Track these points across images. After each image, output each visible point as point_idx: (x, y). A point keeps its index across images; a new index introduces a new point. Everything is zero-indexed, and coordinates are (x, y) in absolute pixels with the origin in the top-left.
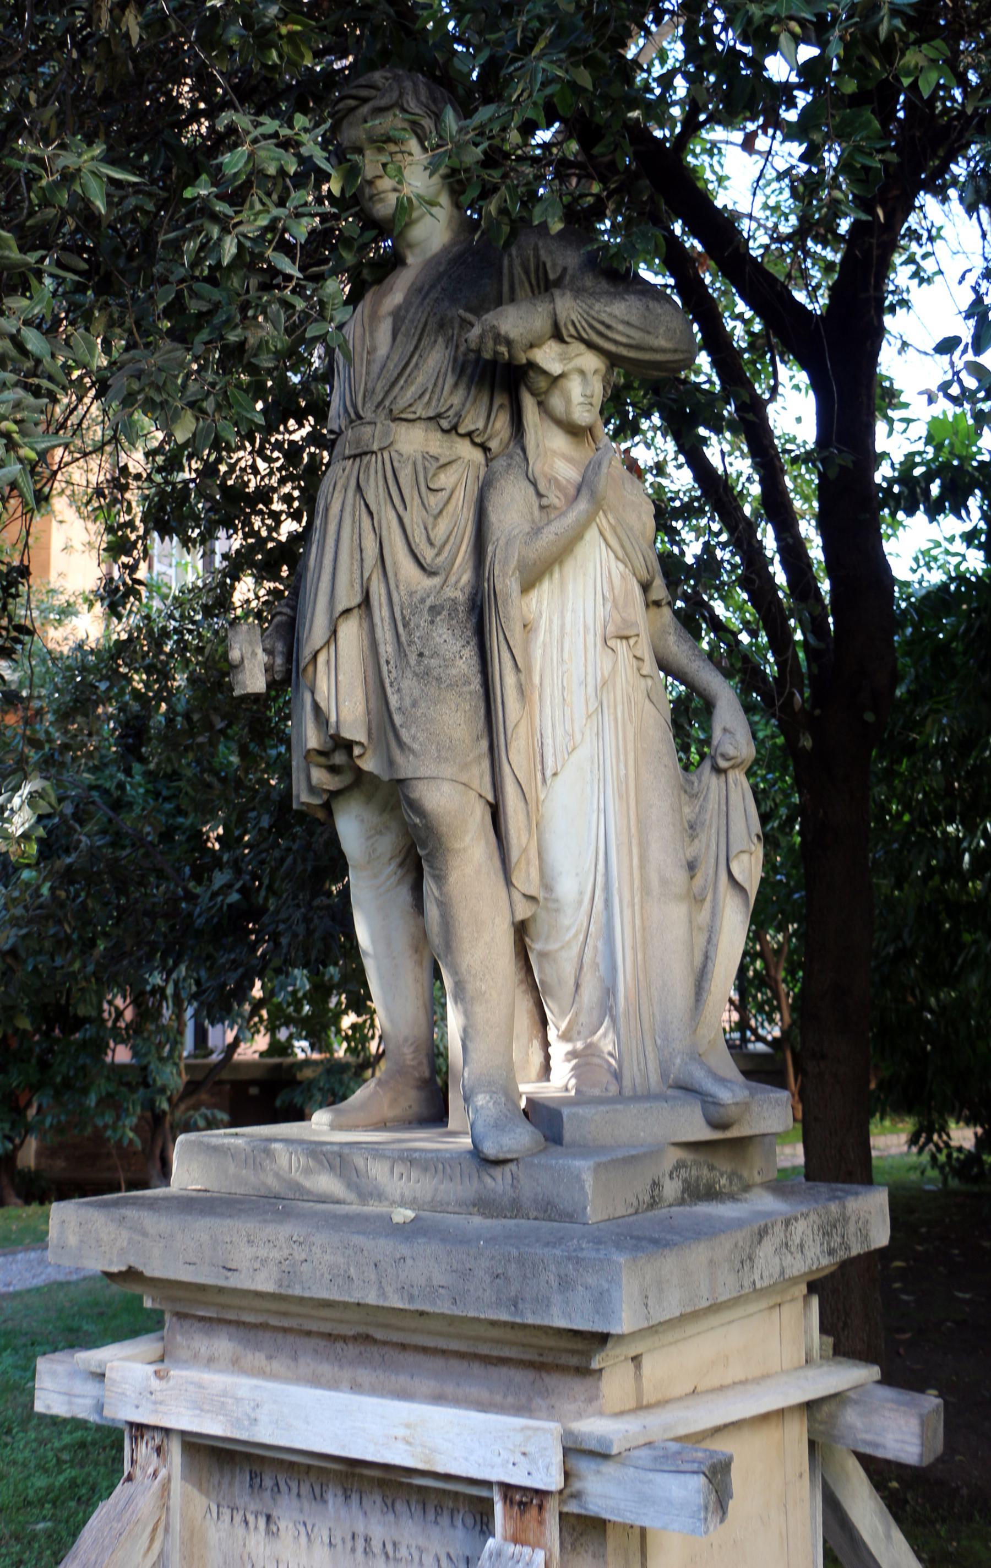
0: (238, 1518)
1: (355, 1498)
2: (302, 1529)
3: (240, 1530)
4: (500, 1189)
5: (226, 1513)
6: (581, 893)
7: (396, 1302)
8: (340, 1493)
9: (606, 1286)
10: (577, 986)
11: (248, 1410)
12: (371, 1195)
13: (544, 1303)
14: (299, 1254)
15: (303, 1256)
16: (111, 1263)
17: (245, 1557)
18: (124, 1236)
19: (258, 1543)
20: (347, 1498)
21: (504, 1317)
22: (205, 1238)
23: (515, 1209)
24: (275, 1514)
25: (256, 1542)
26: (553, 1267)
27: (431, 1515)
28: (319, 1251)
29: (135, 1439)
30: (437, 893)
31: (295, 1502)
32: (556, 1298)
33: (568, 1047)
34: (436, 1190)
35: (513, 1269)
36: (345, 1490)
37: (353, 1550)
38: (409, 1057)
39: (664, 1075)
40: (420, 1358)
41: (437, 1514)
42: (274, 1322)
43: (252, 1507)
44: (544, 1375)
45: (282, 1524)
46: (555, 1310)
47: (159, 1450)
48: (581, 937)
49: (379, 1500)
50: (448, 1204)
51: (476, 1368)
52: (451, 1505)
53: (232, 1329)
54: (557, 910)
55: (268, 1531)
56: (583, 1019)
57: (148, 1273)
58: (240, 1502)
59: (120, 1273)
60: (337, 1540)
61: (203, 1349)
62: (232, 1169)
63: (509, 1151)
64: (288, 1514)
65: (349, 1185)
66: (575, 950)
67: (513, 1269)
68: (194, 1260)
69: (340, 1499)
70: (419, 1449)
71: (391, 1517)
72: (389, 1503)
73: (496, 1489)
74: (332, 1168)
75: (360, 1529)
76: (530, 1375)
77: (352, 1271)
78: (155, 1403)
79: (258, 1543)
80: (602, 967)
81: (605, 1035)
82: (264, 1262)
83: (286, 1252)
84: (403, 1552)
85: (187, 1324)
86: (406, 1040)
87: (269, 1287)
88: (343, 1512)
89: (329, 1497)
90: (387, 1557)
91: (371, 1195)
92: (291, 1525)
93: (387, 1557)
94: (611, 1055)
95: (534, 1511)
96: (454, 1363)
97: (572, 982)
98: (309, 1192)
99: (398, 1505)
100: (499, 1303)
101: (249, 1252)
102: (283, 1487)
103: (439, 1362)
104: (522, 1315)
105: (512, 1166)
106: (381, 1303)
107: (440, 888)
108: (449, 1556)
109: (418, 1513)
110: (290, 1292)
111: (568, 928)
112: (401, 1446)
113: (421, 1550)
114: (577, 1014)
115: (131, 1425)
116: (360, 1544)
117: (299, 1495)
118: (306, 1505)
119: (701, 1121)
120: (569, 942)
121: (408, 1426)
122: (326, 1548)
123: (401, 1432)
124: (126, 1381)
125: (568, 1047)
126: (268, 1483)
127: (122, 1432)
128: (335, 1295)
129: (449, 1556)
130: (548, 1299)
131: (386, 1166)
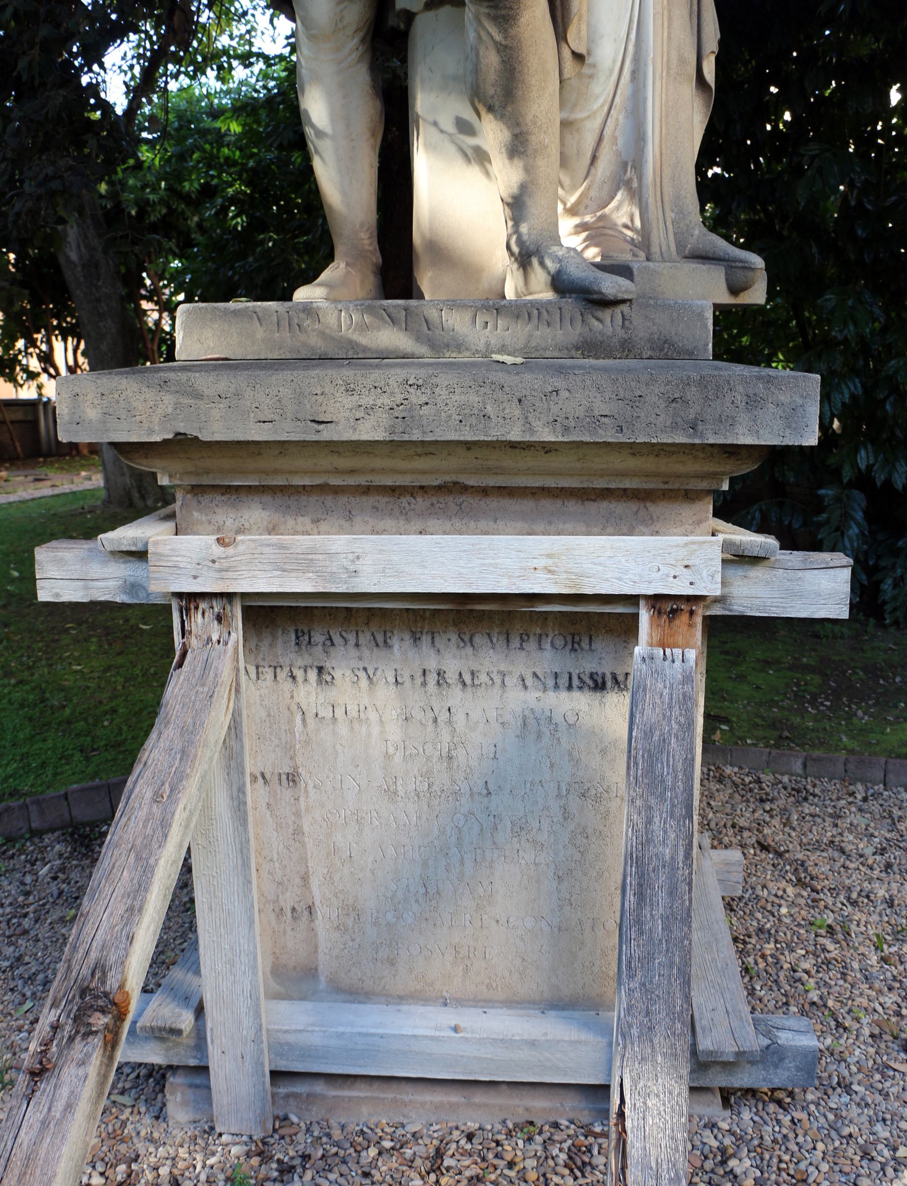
0: (282, 675)
1: (426, 639)
2: (362, 674)
3: (286, 685)
4: (609, 330)
5: (268, 674)
6: (614, 61)
7: (547, 436)
8: (407, 636)
9: (800, 401)
10: (594, 158)
11: (346, 563)
12: (448, 346)
13: (732, 422)
14: (417, 397)
15: (424, 399)
16: (151, 431)
17: (294, 707)
18: (168, 401)
19: (309, 693)
20: (416, 640)
21: (681, 439)
22: (286, 392)
23: (627, 348)
24: (328, 665)
25: (308, 693)
26: (740, 388)
27: (516, 642)
28: (444, 392)
29: (185, 611)
30: (498, 37)
31: (353, 652)
32: (743, 418)
33: (576, 220)
34: (530, 336)
35: (692, 393)
36: (413, 633)
37: (424, 684)
38: (367, 242)
39: (680, 245)
40: (506, 502)
41: (522, 640)
42: (335, 481)
43: (300, 662)
44: (649, 504)
45: (337, 674)
46: (740, 429)
47: (219, 619)
48: (606, 108)
49: (454, 637)
50: (545, 349)
51: (573, 506)
52: (538, 631)
53: (267, 498)
54: (591, 77)
55: (320, 681)
56: (593, 193)
57: (205, 437)
58: (285, 661)
59: (165, 442)
60: (406, 679)
61: (229, 522)
62: (260, 333)
63: (626, 292)
64: (343, 666)
65: (419, 339)
66: (599, 121)
67: (692, 393)
68: (270, 417)
69: (408, 642)
70: (564, 576)
71: (469, 650)
72: (466, 638)
73: (642, 603)
74: (394, 321)
75: (432, 664)
76: (633, 506)
77: (490, 410)
78: (221, 570)
79: (309, 693)
80: (620, 141)
81: (618, 208)
82: (369, 410)
83: (399, 398)
84: (483, 678)
85: (206, 499)
86: (362, 225)
87: (380, 435)
88: (411, 653)
89: (395, 642)
90: (464, 684)
91: (448, 346)
92: (348, 673)
93: (464, 684)
94: (626, 226)
95: (685, 617)
96: (547, 504)
97: (589, 155)
98: (365, 349)
99: (477, 639)
100: (675, 426)
101: (349, 401)
102: (337, 639)
103: (528, 504)
104: (702, 435)
105: (625, 308)
106: (528, 438)
107: (505, 32)
108: (535, 675)
109: (501, 643)
110: (406, 438)
111: (597, 97)
112: (542, 575)
113: (503, 675)
114: (589, 188)
115: (179, 595)
116: (432, 679)
117: (357, 645)
118: (366, 652)
119: (723, 286)
120: (595, 112)
121: (549, 556)
122: (392, 687)
123: (541, 563)
124: (184, 554)
125: (576, 220)
126: (318, 638)
127: (167, 609)
128: (468, 436)
129: (535, 675)
130: (733, 418)
131: (467, 316)
